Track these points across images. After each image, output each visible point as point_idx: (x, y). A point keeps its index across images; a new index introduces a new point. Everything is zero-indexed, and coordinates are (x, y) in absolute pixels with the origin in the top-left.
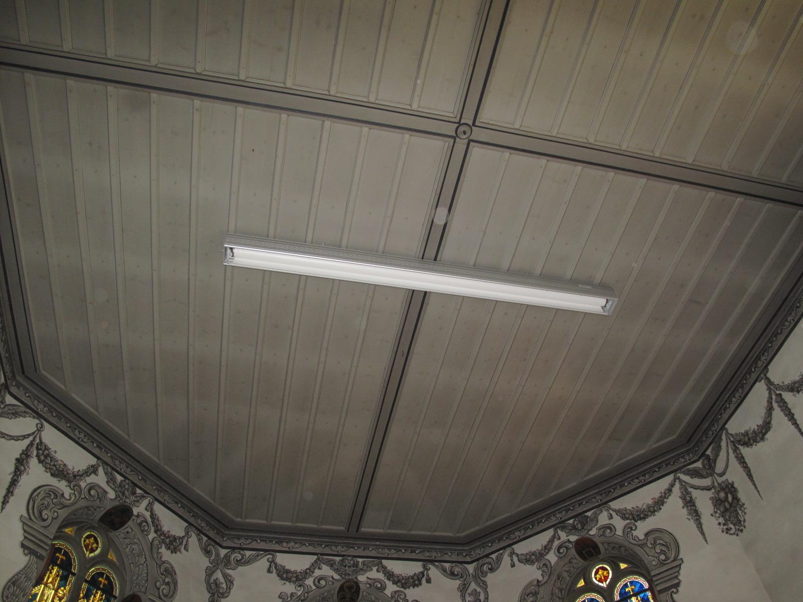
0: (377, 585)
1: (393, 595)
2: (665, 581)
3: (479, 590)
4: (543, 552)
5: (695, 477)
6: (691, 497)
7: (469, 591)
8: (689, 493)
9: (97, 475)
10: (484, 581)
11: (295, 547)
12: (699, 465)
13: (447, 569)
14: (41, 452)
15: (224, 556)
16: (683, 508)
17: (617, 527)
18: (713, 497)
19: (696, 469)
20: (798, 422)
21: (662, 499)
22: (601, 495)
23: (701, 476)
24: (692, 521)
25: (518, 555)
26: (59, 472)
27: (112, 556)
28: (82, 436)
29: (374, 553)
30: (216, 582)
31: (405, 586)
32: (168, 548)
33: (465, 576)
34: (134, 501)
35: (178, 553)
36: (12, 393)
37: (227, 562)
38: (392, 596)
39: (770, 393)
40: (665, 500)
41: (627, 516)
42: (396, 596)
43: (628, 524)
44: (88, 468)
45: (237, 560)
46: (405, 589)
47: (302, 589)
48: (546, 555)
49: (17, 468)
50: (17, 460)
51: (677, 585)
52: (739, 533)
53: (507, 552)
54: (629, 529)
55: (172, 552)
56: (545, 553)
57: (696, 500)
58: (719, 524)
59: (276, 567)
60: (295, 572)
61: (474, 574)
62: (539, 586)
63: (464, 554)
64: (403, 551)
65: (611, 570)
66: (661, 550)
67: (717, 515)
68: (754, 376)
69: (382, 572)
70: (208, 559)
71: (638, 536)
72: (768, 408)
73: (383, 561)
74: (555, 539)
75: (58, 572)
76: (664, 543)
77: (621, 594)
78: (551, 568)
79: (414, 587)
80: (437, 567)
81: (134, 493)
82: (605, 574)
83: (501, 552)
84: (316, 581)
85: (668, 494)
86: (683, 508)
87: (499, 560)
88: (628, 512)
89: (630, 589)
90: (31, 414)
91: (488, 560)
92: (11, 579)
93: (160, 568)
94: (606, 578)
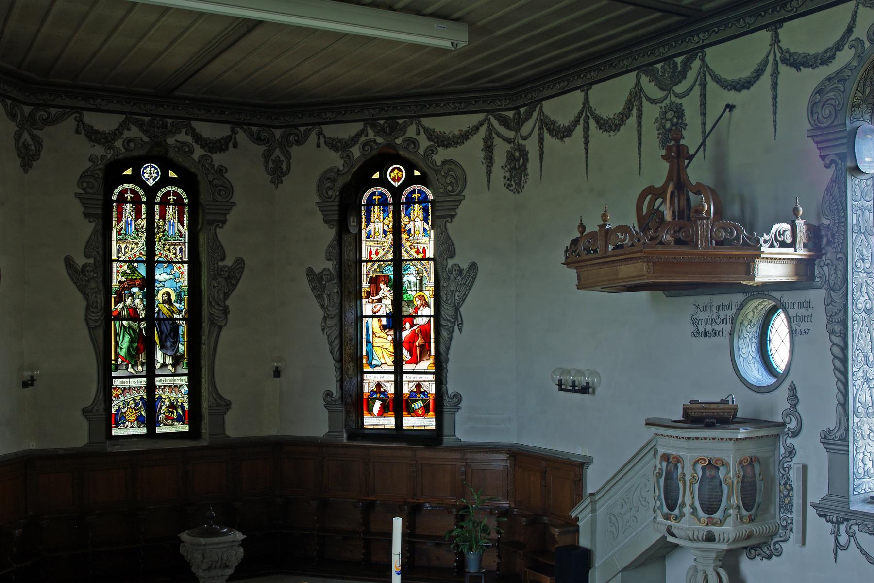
0: (185, 149)
1: (200, 159)
2: (445, 210)
3: (282, 158)
4: (349, 143)
5: (503, 125)
6: (492, 143)
7: (273, 157)
8: (492, 139)
10: (288, 151)
12: (510, 114)
13: (255, 132)
16: (482, 150)
17: (421, 145)
18: (509, 151)
19: (507, 117)
20: (589, 150)
21: (468, 134)
22: (416, 106)
24: (485, 165)
25: (325, 137)
30: (26, 146)
31: (212, 150)
38: (199, 161)
39: (583, 108)
40: (470, 136)
42: (203, 161)
45: (43, 119)
46: (212, 154)
47: (112, 151)
48: (351, 147)
51: (453, 216)
52: (516, 193)
54: (430, 151)
56: (350, 145)
57: (495, 148)
58: (505, 177)
59: (84, 128)
60: (104, 133)
62: (339, 175)
64: (213, 112)
65: (406, 173)
66: (451, 182)
67: (506, 169)
68: (580, 82)
69: (190, 134)
72: (576, 119)
73: (192, 122)
74: (363, 135)
77: (407, 198)
78: (353, 162)
79: (220, 152)
80: (242, 128)
82: (399, 175)
83: (310, 127)
84: (125, 144)
86: (482, 150)
87: (307, 135)
88: (435, 134)
89: (416, 196)
91: (295, 131)
94: (399, 179)
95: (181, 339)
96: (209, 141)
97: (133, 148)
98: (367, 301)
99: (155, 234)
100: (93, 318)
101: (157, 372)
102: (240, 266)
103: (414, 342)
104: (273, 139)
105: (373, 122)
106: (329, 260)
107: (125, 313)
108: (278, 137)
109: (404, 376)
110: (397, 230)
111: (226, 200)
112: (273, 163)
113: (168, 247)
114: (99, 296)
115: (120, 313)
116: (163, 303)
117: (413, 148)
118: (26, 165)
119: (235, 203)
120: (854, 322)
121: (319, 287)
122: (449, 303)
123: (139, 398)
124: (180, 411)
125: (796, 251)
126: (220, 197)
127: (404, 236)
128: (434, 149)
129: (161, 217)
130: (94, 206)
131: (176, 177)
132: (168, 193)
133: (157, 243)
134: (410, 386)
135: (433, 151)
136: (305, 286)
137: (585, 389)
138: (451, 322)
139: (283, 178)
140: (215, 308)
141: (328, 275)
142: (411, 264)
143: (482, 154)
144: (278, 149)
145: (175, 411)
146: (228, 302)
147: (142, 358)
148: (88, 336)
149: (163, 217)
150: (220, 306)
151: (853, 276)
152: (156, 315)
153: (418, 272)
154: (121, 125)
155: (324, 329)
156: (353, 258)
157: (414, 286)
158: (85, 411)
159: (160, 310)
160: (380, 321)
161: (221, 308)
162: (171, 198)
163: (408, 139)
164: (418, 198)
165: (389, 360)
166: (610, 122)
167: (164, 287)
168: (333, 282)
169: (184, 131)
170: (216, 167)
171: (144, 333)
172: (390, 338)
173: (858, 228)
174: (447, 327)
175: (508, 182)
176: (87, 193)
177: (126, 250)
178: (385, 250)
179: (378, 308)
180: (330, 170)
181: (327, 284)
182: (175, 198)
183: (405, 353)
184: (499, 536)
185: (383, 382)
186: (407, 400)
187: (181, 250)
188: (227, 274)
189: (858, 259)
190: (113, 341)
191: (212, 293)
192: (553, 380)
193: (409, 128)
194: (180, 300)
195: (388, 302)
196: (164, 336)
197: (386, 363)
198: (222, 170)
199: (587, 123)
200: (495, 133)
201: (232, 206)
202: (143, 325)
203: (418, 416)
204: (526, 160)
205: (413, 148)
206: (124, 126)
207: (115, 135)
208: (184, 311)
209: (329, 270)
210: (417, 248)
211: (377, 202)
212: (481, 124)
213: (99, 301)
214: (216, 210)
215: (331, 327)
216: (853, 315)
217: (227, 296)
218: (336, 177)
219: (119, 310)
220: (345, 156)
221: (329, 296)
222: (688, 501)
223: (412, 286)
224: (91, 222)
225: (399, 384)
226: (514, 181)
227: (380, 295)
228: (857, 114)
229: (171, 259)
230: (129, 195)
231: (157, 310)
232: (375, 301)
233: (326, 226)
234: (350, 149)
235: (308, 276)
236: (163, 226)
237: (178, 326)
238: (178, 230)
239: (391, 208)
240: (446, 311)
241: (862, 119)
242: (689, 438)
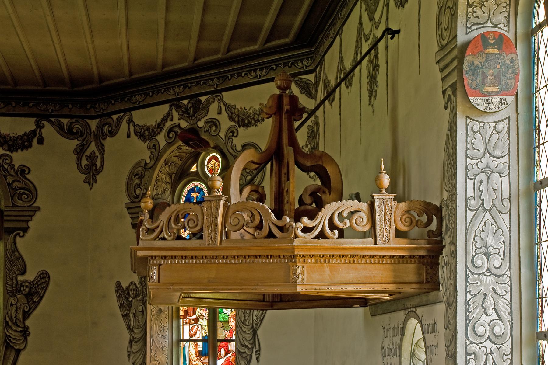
3: (97, 154)
5: (304, 93)
7: (87, 153)
17: (222, 126)
22: (219, 78)
23: (310, 94)
33: (85, 134)
41: (234, 116)
46: (12, 153)
48: (157, 135)
53: (126, 118)
54: (232, 133)
56: (157, 132)
61: (96, 133)
62: (145, 169)
64: (14, 104)
71: (237, 146)
74: (169, 119)
79: (22, 150)
80: (52, 123)
83: (122, 114)
87: (119, 121)
88: (236, 111)
91: (109, 120)
96: (9, 139)
98: (184, 321)
102: (44, 280)
105: (178, 103)
108: (93, 128)
111: (28, 205)
112: (87, 160)
120: (468, 357)
121: (126, 304)
122: (247, 324)
125: (376, 243)
126: (21, 202)
128: (235, 130)
135: (233, 132)
136: (114, 302)
138: (249, 349)
140: (12, 329)
141: (134, 290)
144: (93, 144)
146: (28, 323)
150: (19, 326)
151: (467, 281)
155: (130, 355)
160: (196, 347)
161: (20, 329)
163: (210, 120)
168: (139, 299)
170: (16, 168)
173: (478, 202)
180: (138, 164)
181: (133, 301)
188: (27, 290)
189: (476, 254)
193: (211, 106)
198: (23, 171)
201: (36, 211)
205: (215, 131)
209: (135, 284)
215: (136, 352)
216: (466, 346)
217: (26, 315)
218: (143, 172)
220: (151, 146)
227: (197, 314)
228: (478, 17)
234: (156, 138)
235: (117, 291)
241: (489, 24)
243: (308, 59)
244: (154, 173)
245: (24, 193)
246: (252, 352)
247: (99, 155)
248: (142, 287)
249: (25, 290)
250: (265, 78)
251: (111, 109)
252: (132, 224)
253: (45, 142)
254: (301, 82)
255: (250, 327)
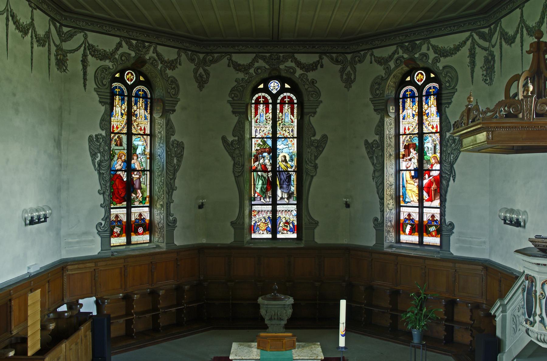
3: (351, 72)
5: (481, 39)
6: (475, 52)
7: (346, 72)
8: (474, 48)
9: (122, 47)
11: (243, 49)
12: (486, 30)
14: (91, 50)
15: (203, 59)
17: (430, 57)
18: (486, 56)
26: (103, 56)
27: (142, 79)
28: (108, 28)
29: (289, 50)
30: (201, 76)
31: (308, 70)
32: (170, 69)
34: (146, 51)
35: (176, 69)
36: (65, 25)
37: (204, 62)
38: (299, 77)
40: (461, 48)
42: (302, 77)
43: (436, 57)
44: (117, 46)
48: (389, 62)
49: (83, 66)
50: (82, 61)
54: (436, 60)
55: (173, 70)
58: (483, 75)
59: (232, 63)
60: (243, 65)
61: (350, 61)
62: (382, 80)
63: (346, 47)
64: (308, 47)
66: (448, 80)
67: (484, 69)
70: (194, 64)
74: (396, 54)
75: (119, 98)
76: (451, 76)
77: (426, 92)
79: (312, 71)
80: (326, 56)
81: (144, 47)
82: (421, 77)
83: (366, 51)
85: (463, 45)
86: (468, 57)
87: (365, 56)
90: (78, 31)
91: (359, 54)
92: (101, 119)
93: (168, 81)
94: (422, 80)
95: (292, 183)
97: (260, 72)
99: (277, 122)
100: (237, 171)
101: (278, 202)
102: (325, 139)
103: (431, 187)
104: (346, 60)
106: (377, 134)
107: (259, 168)
108: (349, 59)
109: (425, 209)
110: (421, 114)
112: (346, 76)
113: (285, 129)
114: (240, 158)
115: (256, 168)
116: (282, 162)
117: (425, 59)
118: (201, 87)
119: (321, 101)
123: (267, 217)
124: (291, 225)
126: (312, 98)
127: (425, 117)
129: (280, 112)
130: (238, 107)
131: (289, 87)
132: (285, 97)
133: (278, 127)
134: (428, 216)
135: (437, 60)
136: (364, 151)
137: (518, 224)
138: (448, 175)
139: (352, 84)
141: (376, 144)
142: (429, 136)
143: (468, 60)
144: (349, 67)
145: (288, 226)
146: (317, 162)
147: (269, 194)
148: (234, 181)
149: (281, 111)
150: (313, 164)
152: (278, 169)
153: (433, 141)
154: (253, 60)
156: (394, 133)
157: (431, 150)
158: (232, 223)
159: (280, 166)
160: (410, 173)
161: (313, 165)
162: (287, 100)
164: (433, 91)
165: (416, 199)
166: (533, 29)
167: (282, 152)
169: (290, 60)
170: (309, 80)
171: (270, 179)
172: (416, 184)
174: (445, 178)
175: (485, 78)
176: (234, 100)
177: (260, 131)
178: (413, 127)
179: (409, 164)
180: (377, 77)
182: (289, 100)
183: (425, 194)
184: (473, 322)
185: (412, 213)
186: (426, 225)
187: (292, 131)
188: (316, 144)
190: (252, 184)
191: (307, 156)
192: (499, 216)
194: (292, 160)
195: (415, 161)
196: (282, 181)
197: (413, 201)
198: (313, 82)
199: (522, 31)
200: (477, 45)
202: (270, 174)
203: (433, 236)
204: (494, 61)
205: (425, 59)
206: (255, 60)
207: (250, 66)
208: (294, 167)
209: (377, 141)
210: (433, 125)
211: (409, 96)
212: (467, 39)
213: (240, 161)
214: (310, 106)
217: (316, 158)
219: (256, 166)
221: (376, 157)
222: (538, 312)
223: (430, 150)
224: (236, 116)
225: (421, 214)
226: (489, 77)
229: (287, 136)
230: (287, 99)
231: (278, 166)
232: (407, 160)
233: (375, 113)
234: (389, 63)
235: (365, 145)
236: (282, 117)
237: (290, 176)
238: (291, 119)
239: (417, 99)
240: (445, 167)
242: (538, 264)
243: (483, 20)
244: (387, 82)
245: (313, 94)
246: (450, 176)
247: (353, 73)
248: (381, 143)
249: (315, 145)
250: (457, 31)
251: (360, 48)
252: (374, 109)
253: (324, 66)
254: (480, 33)
255: (449, 163)
